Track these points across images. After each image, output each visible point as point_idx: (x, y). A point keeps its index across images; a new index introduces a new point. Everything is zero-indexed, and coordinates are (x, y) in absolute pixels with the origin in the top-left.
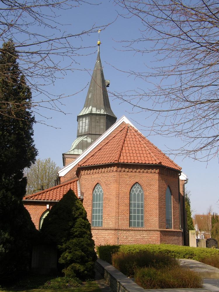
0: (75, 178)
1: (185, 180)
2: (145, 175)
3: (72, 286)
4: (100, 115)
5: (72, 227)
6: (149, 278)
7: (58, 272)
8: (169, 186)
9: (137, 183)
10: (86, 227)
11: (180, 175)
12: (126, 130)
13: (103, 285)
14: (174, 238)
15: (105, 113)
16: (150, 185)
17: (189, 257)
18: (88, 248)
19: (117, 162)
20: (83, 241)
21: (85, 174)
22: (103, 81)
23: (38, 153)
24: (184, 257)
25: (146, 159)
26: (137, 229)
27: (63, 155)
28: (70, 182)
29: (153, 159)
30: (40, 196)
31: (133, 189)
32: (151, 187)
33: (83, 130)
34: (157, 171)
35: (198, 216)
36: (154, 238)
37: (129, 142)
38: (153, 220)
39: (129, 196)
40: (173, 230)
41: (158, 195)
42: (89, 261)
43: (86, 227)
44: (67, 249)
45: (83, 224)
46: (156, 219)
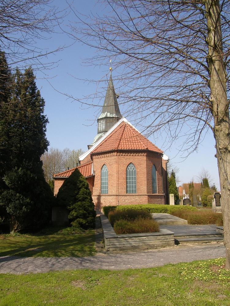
0: (90, 161)
1: (167, 160)
2: (136, 157)
3: (76, 233)
4: (113, 117)
5: (77, 194)
6: (121, 227)
7: (68, 224)
8: (154, 164)
9: (131, 163)
10: (87, 194)
11: (163, 156)
12: (124, 126)
13: (98, 232)
14: (158, 200)
15: (116, 116)
16: (140, 164)
17: (164, 212)
18: (88, 208)
19: (116, 149)
20: (86, 203)
21: (96, 158)
22: (115, 94)
23: (49, 143)
24: (161, 212)
25: (137, 146)
26: (132, 194)
27: (88, 146)
28: (87, 164)
29: (142, 146)
30: (65, 174)
31: (128, 167)
32: (141, 166)
33: (102, 129)
34: (145, 154)
35: (185, 184)
36: (144, 200)
37: (125, 135)
38: (143, 188)
39: (125, 172)
40: (157, 194)
41: (146, 171)
42: (90, 217)
43: (87, 194)
44: (74, 209)
45: (85, 192)
46: (145, 187)
